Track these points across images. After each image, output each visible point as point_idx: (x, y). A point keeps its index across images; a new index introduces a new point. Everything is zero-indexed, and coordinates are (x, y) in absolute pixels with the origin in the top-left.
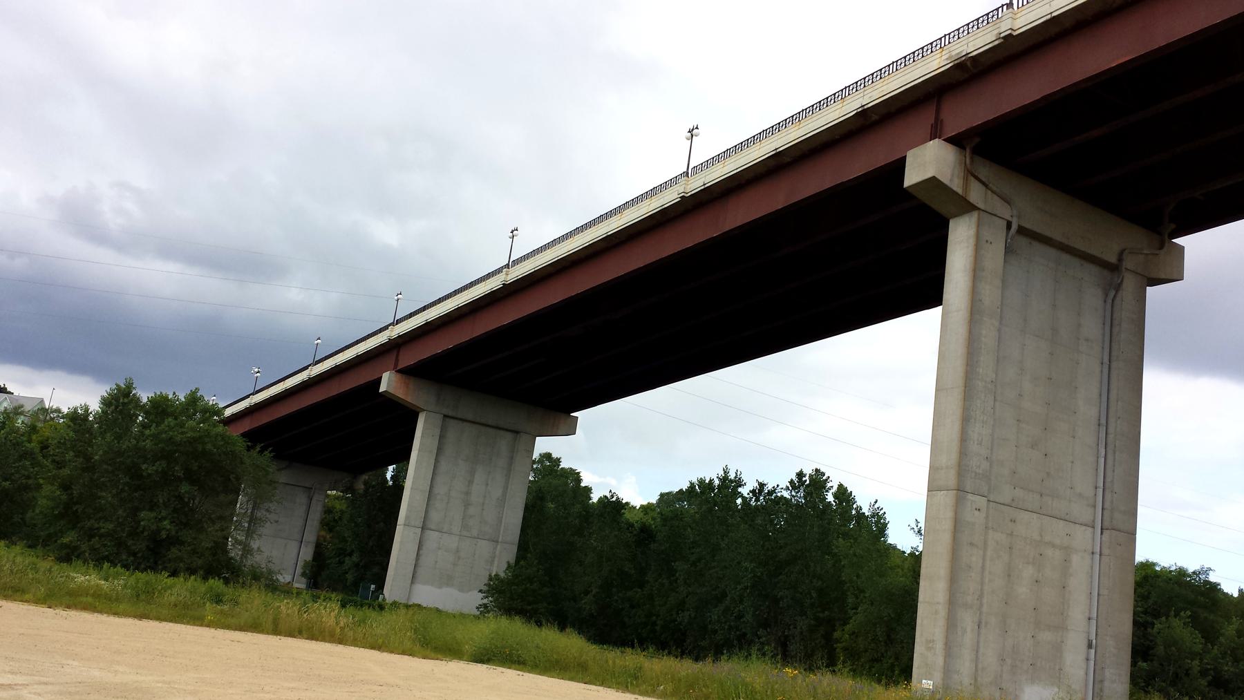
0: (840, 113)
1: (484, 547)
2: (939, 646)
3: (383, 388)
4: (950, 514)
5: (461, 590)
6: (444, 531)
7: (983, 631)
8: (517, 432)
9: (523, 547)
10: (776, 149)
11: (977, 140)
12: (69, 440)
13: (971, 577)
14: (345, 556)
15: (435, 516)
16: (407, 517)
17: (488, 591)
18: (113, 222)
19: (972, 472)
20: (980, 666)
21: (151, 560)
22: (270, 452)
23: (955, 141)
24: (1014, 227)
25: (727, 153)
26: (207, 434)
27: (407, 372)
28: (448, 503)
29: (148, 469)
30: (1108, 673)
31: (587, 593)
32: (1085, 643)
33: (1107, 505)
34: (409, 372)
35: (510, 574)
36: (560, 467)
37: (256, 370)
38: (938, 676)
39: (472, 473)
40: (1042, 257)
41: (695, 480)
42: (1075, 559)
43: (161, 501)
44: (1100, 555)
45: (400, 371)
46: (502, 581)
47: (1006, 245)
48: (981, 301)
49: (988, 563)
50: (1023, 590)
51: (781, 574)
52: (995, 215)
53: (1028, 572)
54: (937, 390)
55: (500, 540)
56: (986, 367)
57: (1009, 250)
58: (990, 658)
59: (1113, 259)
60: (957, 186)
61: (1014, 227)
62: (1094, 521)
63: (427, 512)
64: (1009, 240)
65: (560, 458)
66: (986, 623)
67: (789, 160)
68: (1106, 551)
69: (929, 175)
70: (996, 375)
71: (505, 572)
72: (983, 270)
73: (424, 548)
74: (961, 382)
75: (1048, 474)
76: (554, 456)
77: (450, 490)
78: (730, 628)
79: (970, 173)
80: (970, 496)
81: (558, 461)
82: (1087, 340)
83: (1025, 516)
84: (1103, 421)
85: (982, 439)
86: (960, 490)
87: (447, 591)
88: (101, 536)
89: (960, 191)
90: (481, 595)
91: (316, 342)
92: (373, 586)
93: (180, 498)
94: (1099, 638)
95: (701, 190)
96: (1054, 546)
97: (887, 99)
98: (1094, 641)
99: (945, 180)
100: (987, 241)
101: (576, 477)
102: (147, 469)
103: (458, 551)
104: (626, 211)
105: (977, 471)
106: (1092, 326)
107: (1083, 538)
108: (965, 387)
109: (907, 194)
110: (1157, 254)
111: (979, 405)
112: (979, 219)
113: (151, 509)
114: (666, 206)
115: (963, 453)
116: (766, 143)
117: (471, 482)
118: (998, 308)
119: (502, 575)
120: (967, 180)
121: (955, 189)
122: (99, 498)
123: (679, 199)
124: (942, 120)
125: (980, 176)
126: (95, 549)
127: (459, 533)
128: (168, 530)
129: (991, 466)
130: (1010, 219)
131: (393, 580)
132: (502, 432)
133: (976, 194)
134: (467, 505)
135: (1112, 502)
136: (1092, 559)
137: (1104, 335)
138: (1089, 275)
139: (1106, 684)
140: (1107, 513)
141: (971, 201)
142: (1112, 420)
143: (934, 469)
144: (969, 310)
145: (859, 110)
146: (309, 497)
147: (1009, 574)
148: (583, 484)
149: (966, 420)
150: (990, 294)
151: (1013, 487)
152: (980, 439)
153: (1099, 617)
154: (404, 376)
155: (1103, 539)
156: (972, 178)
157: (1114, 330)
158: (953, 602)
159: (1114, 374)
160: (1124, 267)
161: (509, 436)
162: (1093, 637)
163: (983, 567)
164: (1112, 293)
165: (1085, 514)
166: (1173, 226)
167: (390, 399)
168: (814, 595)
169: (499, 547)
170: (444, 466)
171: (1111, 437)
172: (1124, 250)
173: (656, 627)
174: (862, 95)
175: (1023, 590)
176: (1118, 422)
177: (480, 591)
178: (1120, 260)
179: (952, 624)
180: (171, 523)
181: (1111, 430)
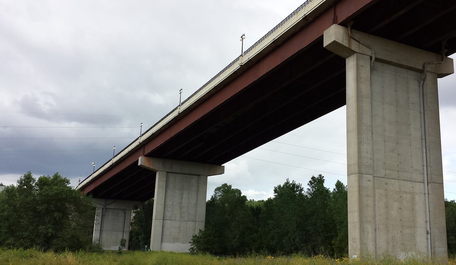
0: (296, 19)
1: (191, 224)
2: (358, 241)
3: (139, 164)
4: (357, 184)
5: (183, 243)
6: (173, 220)
7: (377, 232)
8: (199, 175)
9: (207, 222)
10: (274, 39)
11: (352, 22)
12: (6, 200)
13: (368, 209)
14: (139, 235)
15: (168, 214)
16: (156, 216)
17: (193, 242)
18: (45, 108)
19: (365, 165)
20: (378, 247)
21: (46, 246)
22: (91, 195)
23: (343, 24)
24: (373, 58)
25: (256, 44)
26: (62, 191)
27: (149, 156)
28: (173, 208)
29: (39, 208)
30: (437, 244)
31: (234, 238)
32: (426, 232)
33: (429, 173)
34: (150, 156)
35: (201, 234)
36: (232, 189)
37: (94, 163)
38: (358, 252)
39: (182, 194)
40: (389, 71)
41: (276, 186)
42: (417, 197)
43: (47, 221)
44: (428, 194)
45: (145, 156)
46: (198, 237)
47: (370, 67)
48: (361, 92)
49: (376, 203)
50: (394, 213)
51: (309, 220)
52: (364, 54)
53: (396, 205)
54: (347, 132)
55: (197, 221)
56: (366, 120)
57: (372, 69)
58: (382, 243)
59: (421, 68)
60: (345, 44)
61: (373, 58)
62: (424, 180)
63: (164, 213)
64: (372, 64)
65: (231, 185)
66: (379, 229)
67: (280, 43)
68: (430, 192)
69: (333, 40)
70: (372, 122)
71: (198, 233)
72: (361, 78)
73: (165, 228)
74: (356, 128)
75: (400, 162)
76: (228, 185)
77: (173, 203)
78: (292, 245)
79: (351, 38)
80: (364, 175)
81: (231, 186)
82: (413, 103)
83: (393, 181)
84: (424, 137)
85: (368, 151)
86: (360, 173)
87: (177, 244)
88: (24, 238)
89: (347, 46)
90: (190, 244)
91: (114, 148)
92: (146, 246)
93: (55, 219)
94: (431, 229)
95: (248, 61)
96: (406, 193)
97: (316, 8)
98: (429, 231)
99: (340, 42)
100: (362, 66)
101: (239, 192)
102: (39, 208)
103: (180, 227)
104: (221, 75)
105: (367, 164)
106: (414, 97)
107: (419, 188)
108: (358, 129)
109: (325, 49)
110: (441, 63)
111: (365, 136)
112: (357, 57)
113: (44, 225)
114: (235, 70)
115: (360, 157)
116: (271, 37)
117: (182, 198)
118: (370, 94)
119: (198, 235)
120: (350, 41)
121: (345, 45)
122: (21, 222)
123: (240, 66)
124: (337, 16)
125: (356, 38)
126: (22, 244)
127: (179, 220)
128: (51, 233)
129: (373, 161)
130: (371, 55)
131: (153, 242)
132: (192, 176)
133: (354, 46)
134: (181, 208)
135: (431, 171)
136: (425, 196)
137: (420, 101)
138: (411, 75)
139: (436, 248)
140: (429, 176)
141: (353, 49)
142: (427, 137)
143: (349, 166)
144: (356, 96)
145: (303, 17)
146: (124, 213)
147: (387, 207)
148: (242, 195)
149: (360, 143)
150: (365, 88)
151: (385, 170)
152: (367, 150)
153: (431, 220)
154: (148, 158)
155: (429, 187)
156: (352, 39)
157: (424, 98)
158: (361, 222)
159: (426, 116)
160: (426, 71)
161: (196, 177)
162: (429, 229)
163: (374, 205)
164: (422, 82)
165: (420, 178)
166: (446, 50)
167: (145, 168)
168: (322, 227)
169: (197, 224)
170: (169, 193)
171: (427, 144)
172: (425, 63)
173: (248, 248)
174: (304, 10)
175: (394, 213)
176: (430, 137)
177: (190, 243)
178: (424, 68)
179: (362, 231)
180: (52, 229)
181: (427, 141)
